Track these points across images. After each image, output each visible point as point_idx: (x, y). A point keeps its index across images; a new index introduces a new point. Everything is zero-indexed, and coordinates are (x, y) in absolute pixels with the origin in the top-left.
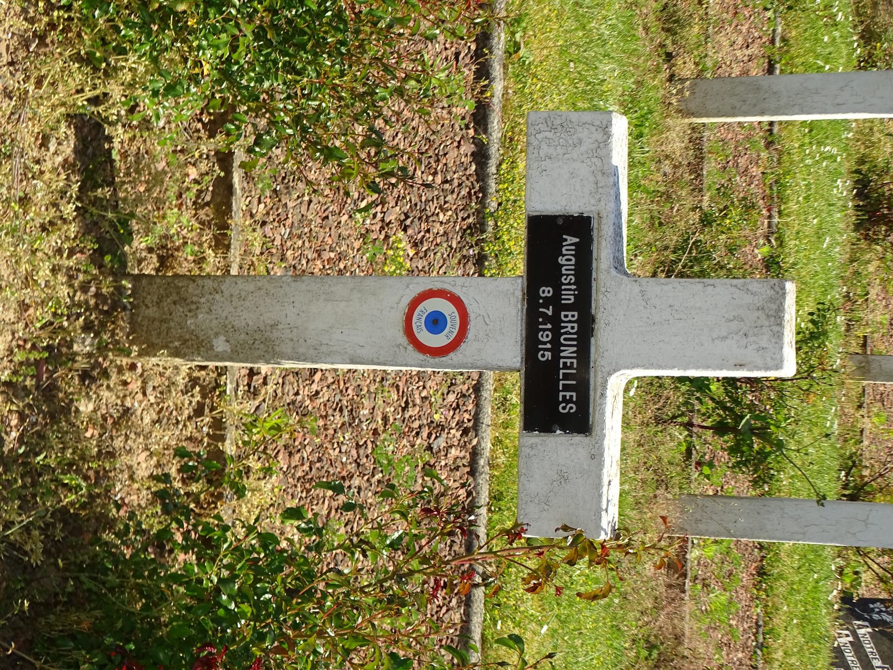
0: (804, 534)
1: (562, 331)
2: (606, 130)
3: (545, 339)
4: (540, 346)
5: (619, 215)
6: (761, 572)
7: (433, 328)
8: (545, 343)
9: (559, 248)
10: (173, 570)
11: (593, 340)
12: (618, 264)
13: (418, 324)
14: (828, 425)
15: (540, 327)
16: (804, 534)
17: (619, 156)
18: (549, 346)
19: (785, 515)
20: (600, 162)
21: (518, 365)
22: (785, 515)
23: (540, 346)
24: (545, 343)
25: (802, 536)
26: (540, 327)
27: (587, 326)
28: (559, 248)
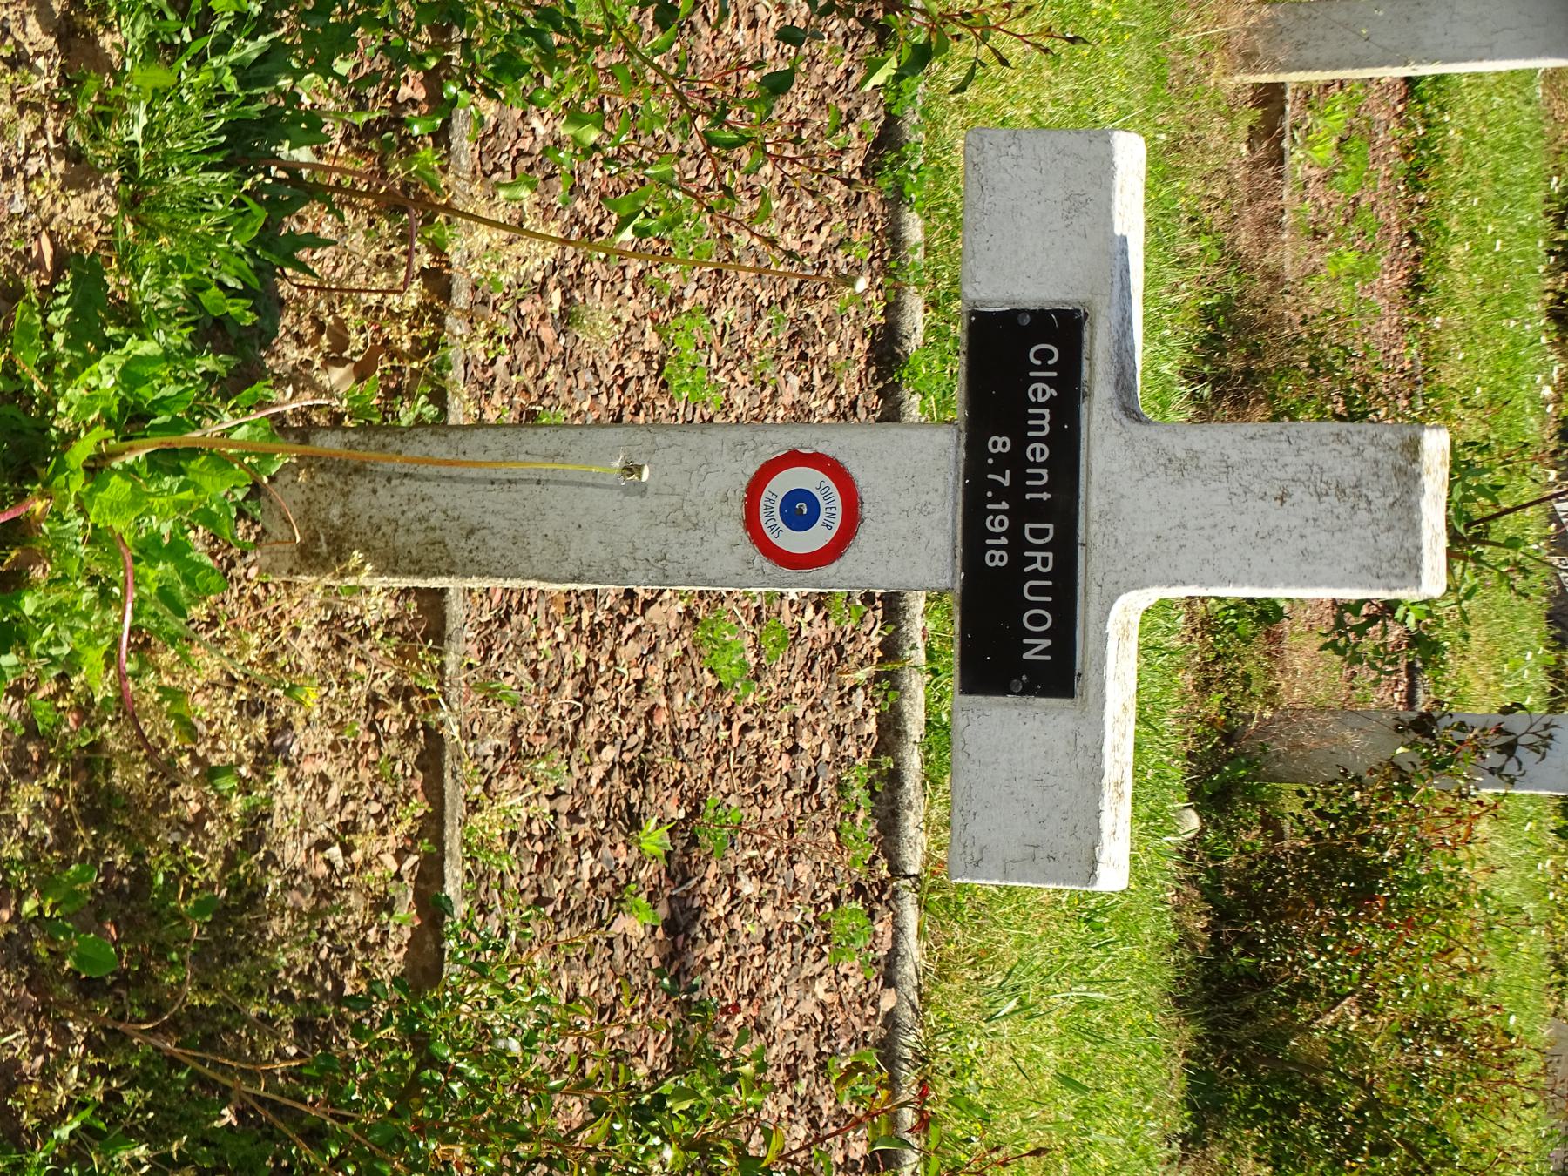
0: (1491, 46)
1: (1027, 570)
2: (1104, 171)
3: (998, 529)
4: (988, 542)
5: (1126, 320)
6: (1416, 285)
7: (803, 511)
8: (997, 536)
9: (1024, 370)
10: (225, 176)
11: (1083, 408)
12: (1130, 411)
13: (771, 523)
14: (1499, 242)
15: (989, 506)
16: (1491, 46)
17: (1129, 215)
18: (1004, 541)
19: (1456, 17)
20: (1107, 221)
21: (946, 582)
22: (1456, 17)
23: (988, 542)
24: (997, 536)
25: (1487, 50)
26: (989, 506)
27: (1066, 547)
28: (1024, 370)
